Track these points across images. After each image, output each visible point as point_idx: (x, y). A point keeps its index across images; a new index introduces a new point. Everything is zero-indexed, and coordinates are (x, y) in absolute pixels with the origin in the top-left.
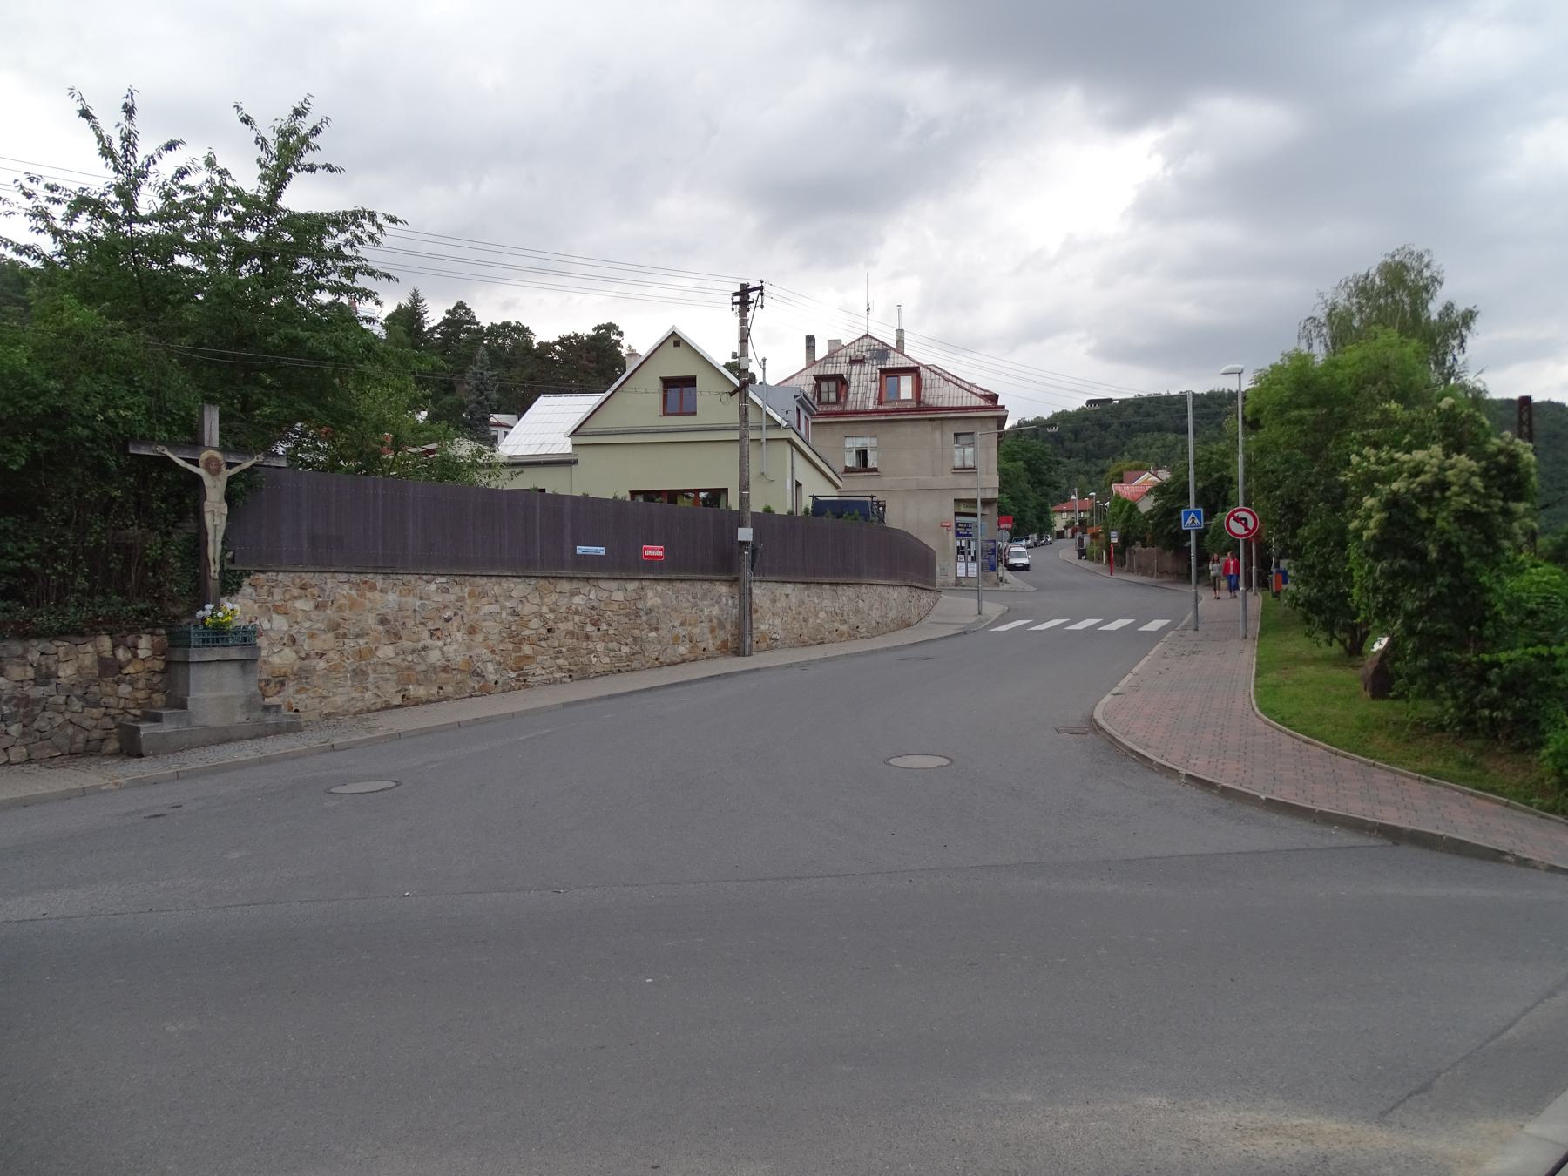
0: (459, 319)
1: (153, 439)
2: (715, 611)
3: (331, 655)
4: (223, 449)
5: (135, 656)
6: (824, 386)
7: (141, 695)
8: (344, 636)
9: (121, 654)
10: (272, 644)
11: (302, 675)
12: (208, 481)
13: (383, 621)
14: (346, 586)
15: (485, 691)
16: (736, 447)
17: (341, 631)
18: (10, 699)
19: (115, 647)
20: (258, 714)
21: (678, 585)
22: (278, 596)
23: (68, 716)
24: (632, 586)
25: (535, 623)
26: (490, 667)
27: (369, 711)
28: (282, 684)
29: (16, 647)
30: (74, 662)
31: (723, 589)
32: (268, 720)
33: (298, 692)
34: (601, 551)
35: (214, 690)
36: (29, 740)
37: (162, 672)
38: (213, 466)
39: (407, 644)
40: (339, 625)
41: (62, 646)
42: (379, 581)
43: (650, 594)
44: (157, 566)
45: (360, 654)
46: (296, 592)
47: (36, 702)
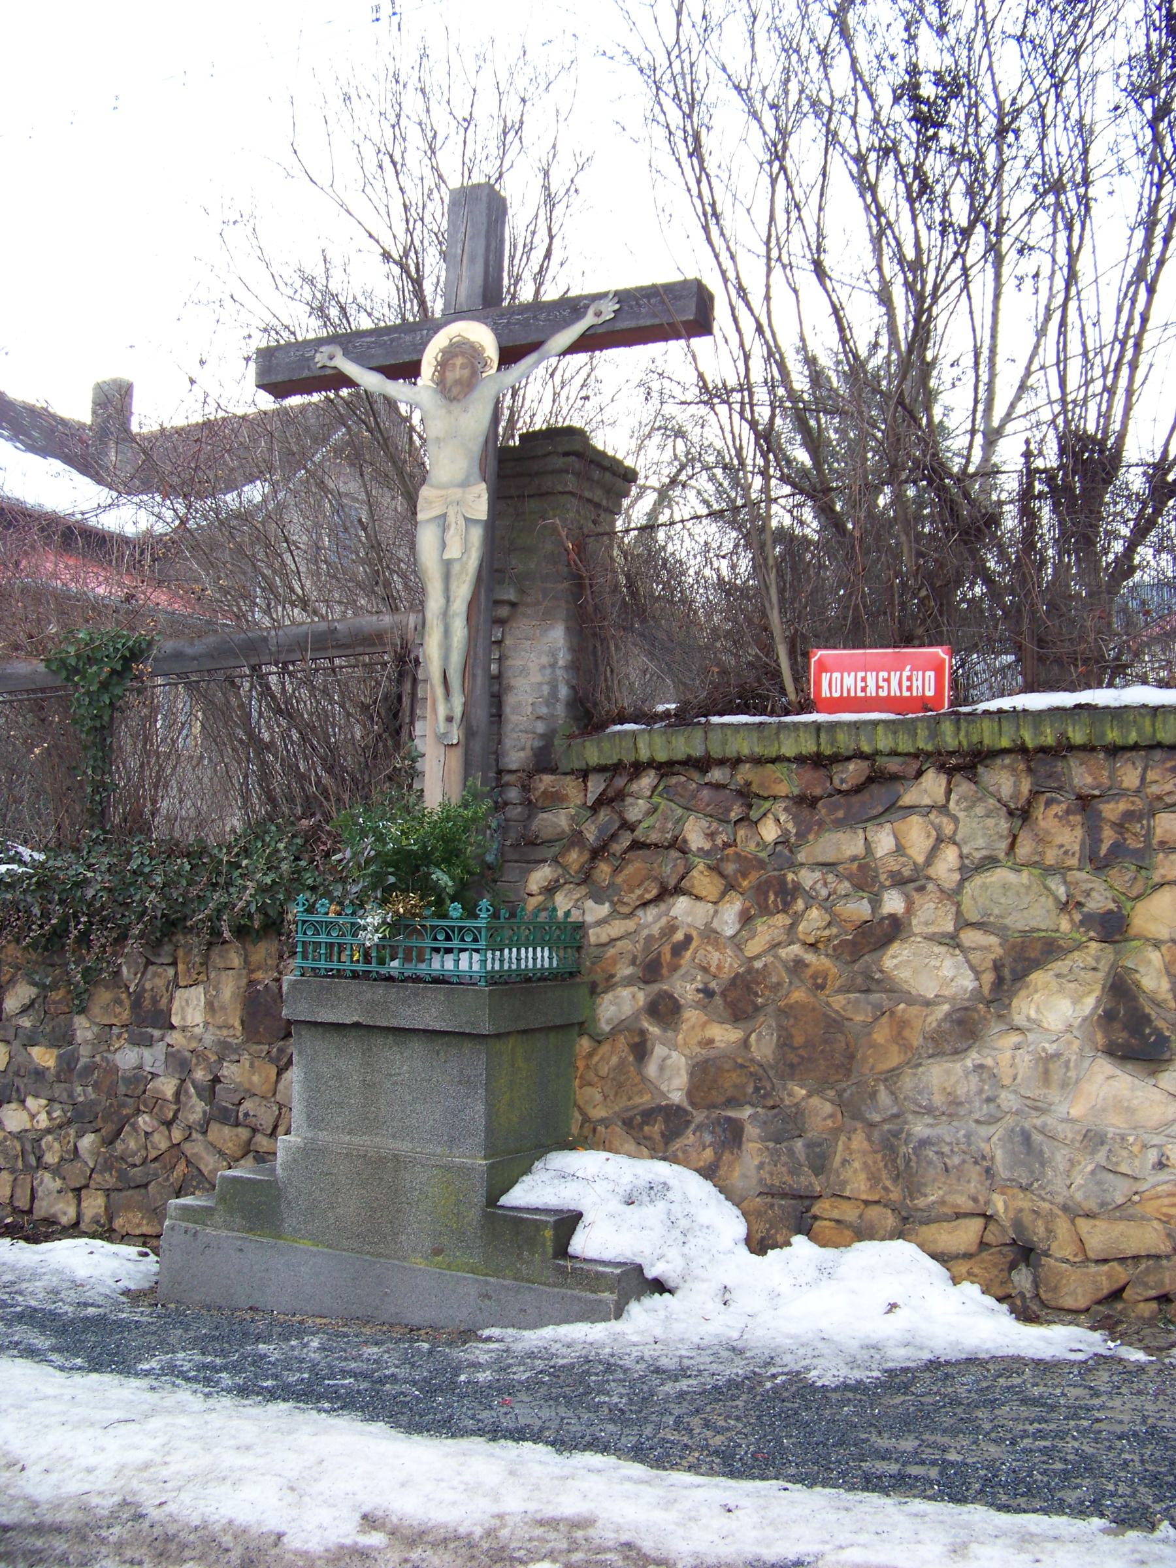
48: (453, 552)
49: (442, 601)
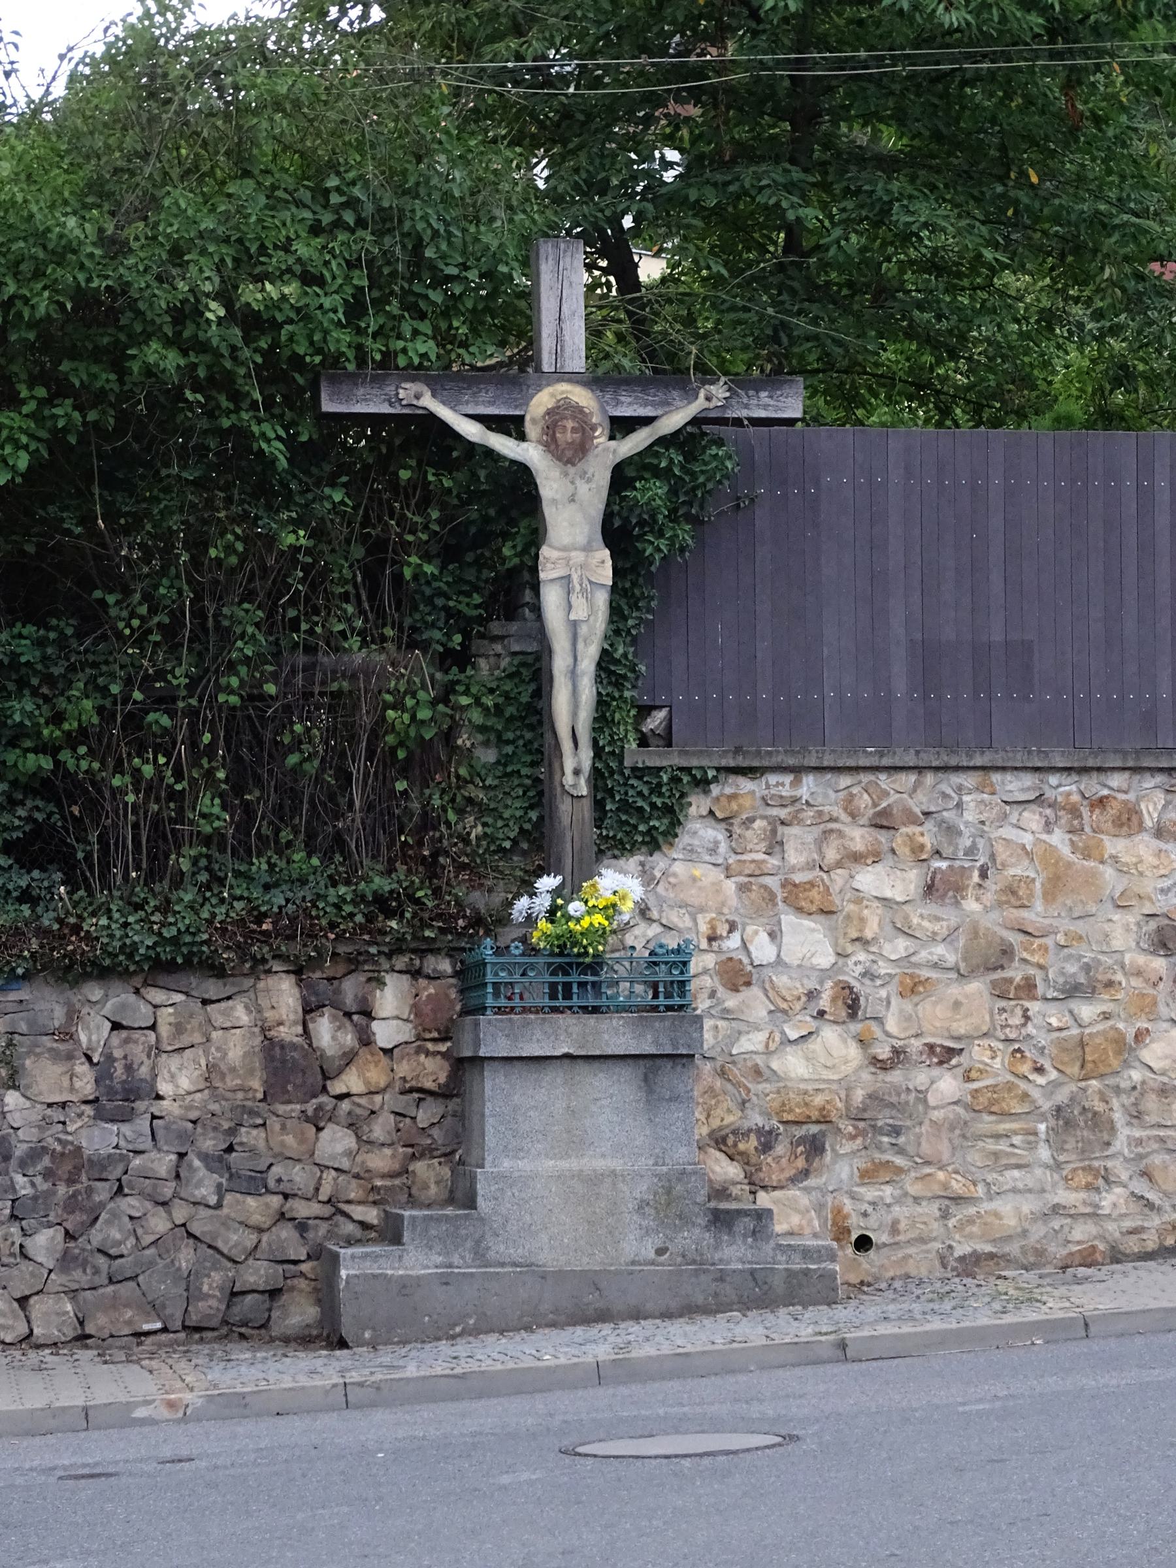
1: (388, 361)
3: (978, 1054)
4: (602, 376)
5: (366, 1040)
7: (381, 1161)
8: (1028, 988)
9: (328, 1034)
10: (780, 1013)
11: (881, 1120)
12: (551, 484)
14: (1032, 818)
17: (1016, 973)
18: (35, 1154)
19: (309, 1010)
20: (693, 1237)
22: (798, 848)
23: (180, 1213)
27: (1117, 1256)
28: (815, 1147)
29: (47, 1003)
30: (200, 1048)
32: (722, 1249)
33: (867, 1176)
35: (564, 1153)
36: (79, 1277)
37: (444, 1094)
38: (567, 436)
40: (1007, 952)
41: (166, 1004)
44: (428, 758)
45: (1083, 1056)
46: (859, 837)
47: (98, 1168)
48: (580, 611)
49: (570, 660)
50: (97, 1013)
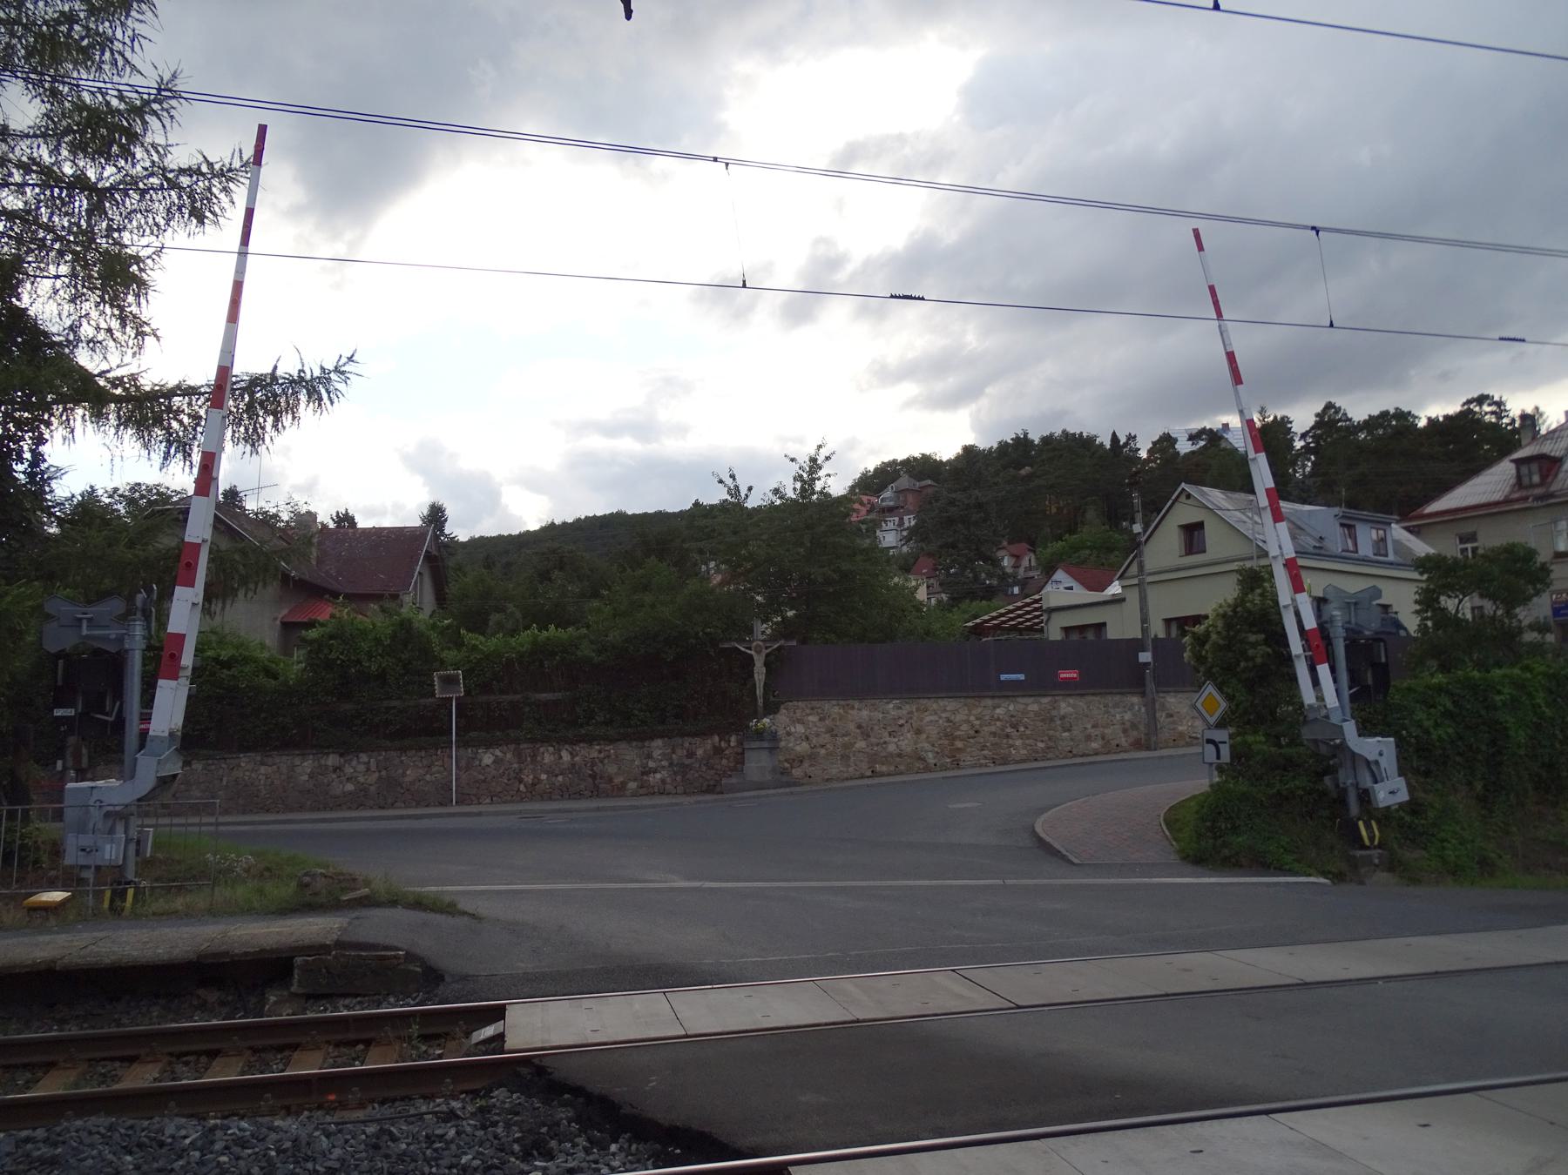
0: (1329, 421)
2: (1128, 716)
6: (1524, 470)
11: (812, 757)
13: (859, 727)
15: (927, 769)
16: (1136, 590)
21: (1090, 698)
24: (1045, 700)
25: (965, 727)
26: (930, 755)
31: (1135, 700)
32: (782, 778)
34: (1022, 677)
35: (758, 763)
39: (873, 740)
41: (698, 740)
42: (857, 705)
43: (1063, 705)
45: (845, 746)
50: (687, 742)
